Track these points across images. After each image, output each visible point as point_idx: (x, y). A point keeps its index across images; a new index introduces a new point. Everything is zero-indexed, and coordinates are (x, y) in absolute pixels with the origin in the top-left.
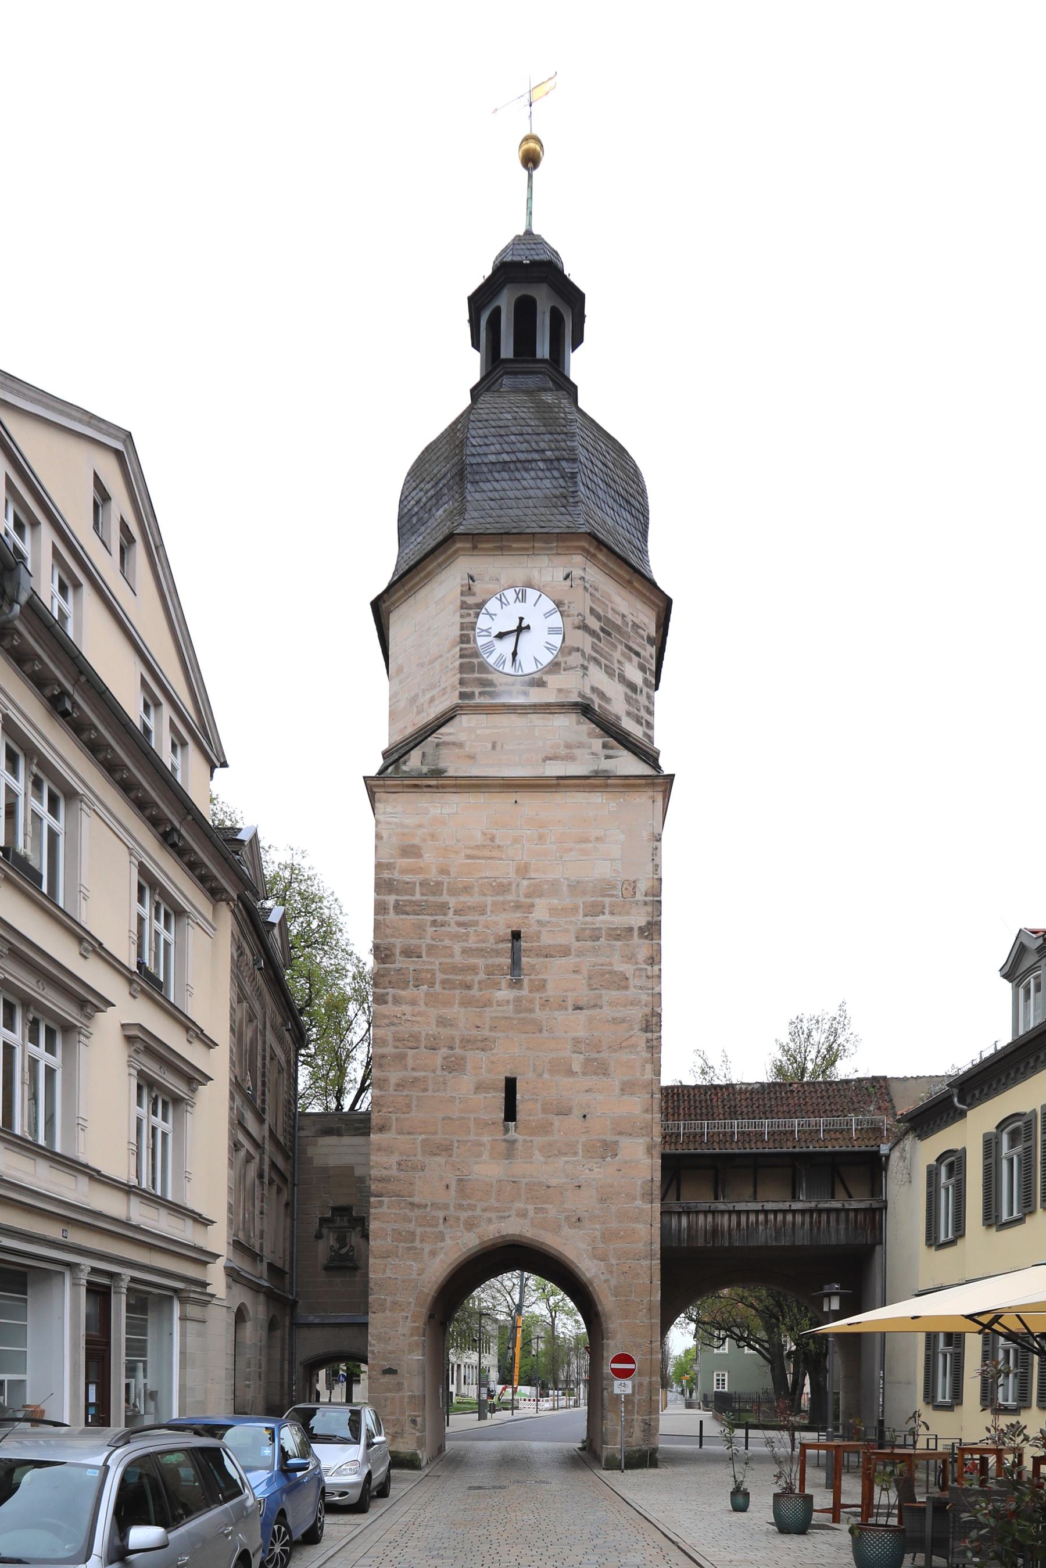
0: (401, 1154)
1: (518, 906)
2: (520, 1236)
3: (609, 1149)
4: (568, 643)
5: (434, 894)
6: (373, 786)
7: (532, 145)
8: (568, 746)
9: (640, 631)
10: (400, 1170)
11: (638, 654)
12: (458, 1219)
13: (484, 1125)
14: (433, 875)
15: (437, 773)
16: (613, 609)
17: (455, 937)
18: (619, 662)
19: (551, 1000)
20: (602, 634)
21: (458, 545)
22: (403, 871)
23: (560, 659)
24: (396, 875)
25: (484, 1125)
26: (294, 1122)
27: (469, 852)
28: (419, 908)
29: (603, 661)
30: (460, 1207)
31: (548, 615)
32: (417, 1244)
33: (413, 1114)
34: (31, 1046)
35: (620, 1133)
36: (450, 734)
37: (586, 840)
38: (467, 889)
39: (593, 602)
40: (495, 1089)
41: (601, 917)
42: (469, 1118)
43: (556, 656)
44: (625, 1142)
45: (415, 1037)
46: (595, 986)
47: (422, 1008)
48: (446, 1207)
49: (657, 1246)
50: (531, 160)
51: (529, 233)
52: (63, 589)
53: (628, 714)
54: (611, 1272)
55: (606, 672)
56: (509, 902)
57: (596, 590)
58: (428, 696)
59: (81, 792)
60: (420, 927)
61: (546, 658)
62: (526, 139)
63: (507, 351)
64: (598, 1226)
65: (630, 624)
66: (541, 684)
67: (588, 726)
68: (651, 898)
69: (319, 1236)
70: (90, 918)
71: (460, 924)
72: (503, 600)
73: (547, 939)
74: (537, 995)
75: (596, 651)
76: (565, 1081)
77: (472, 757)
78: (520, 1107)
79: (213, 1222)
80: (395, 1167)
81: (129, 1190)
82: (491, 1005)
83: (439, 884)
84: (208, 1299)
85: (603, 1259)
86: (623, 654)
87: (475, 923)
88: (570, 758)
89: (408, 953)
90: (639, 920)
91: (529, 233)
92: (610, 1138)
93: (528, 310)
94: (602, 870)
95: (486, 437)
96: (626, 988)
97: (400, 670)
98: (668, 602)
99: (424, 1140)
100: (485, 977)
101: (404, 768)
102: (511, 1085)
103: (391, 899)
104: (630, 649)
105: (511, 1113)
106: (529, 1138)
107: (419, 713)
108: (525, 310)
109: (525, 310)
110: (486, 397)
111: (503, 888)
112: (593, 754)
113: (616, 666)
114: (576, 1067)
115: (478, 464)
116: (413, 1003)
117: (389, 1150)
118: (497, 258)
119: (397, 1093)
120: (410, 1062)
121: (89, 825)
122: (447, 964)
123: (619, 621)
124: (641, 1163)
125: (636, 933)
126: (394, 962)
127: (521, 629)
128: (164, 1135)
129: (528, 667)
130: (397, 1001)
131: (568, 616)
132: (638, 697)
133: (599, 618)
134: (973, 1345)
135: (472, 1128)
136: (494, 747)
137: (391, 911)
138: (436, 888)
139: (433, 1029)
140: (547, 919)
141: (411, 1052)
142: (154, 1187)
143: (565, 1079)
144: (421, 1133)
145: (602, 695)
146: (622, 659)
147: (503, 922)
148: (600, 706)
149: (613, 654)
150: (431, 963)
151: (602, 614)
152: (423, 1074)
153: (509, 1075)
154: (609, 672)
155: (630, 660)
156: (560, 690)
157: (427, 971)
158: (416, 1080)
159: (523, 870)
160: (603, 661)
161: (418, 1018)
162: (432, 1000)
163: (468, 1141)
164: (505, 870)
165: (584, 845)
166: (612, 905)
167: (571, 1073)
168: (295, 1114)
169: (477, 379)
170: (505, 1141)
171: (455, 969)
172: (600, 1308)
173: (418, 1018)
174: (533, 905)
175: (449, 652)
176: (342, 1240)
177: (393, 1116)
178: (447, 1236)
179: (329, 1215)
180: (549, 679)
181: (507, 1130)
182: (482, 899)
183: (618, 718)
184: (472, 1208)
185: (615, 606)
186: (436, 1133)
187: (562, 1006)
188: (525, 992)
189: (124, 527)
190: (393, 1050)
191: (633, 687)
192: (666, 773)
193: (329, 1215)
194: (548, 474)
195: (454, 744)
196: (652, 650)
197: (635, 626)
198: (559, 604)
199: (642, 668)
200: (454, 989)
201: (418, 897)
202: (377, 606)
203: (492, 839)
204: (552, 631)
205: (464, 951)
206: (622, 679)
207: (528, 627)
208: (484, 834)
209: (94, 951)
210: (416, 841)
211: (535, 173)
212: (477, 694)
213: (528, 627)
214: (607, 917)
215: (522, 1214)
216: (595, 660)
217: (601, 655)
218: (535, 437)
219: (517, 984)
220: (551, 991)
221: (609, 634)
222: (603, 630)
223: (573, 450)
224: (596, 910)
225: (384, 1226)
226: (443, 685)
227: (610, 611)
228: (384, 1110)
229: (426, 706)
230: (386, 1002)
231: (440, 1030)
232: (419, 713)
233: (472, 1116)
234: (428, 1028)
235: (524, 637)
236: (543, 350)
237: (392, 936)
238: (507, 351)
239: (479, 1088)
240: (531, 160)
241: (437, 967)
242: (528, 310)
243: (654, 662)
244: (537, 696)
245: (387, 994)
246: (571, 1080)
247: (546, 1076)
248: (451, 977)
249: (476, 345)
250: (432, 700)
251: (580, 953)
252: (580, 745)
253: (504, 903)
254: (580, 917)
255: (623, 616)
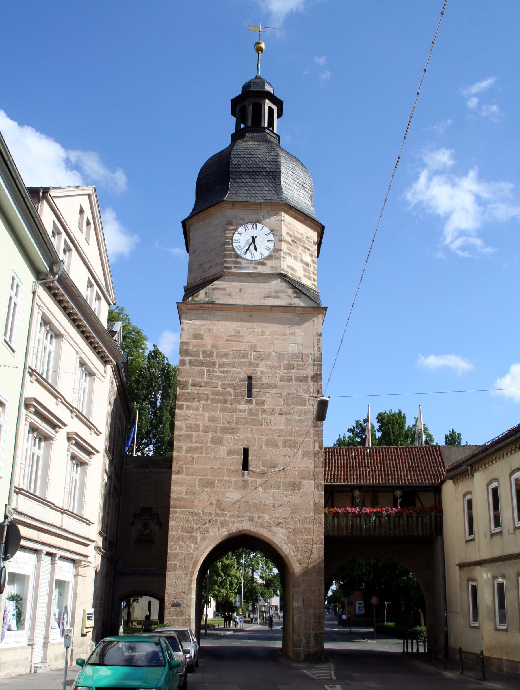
0: (188, 486)
1: (251, 364)
2: (249, 531)
3: (295, 486)
4: (276, 247)
5: (209, 357)
8: (276, 292)
9: (310, 240)
10: (186, 494)
11: (309, 250)
12: (217, 521)
13: (231, 472)
14: (209, 348)
15: (212, 303)
16: (297, 232)
17: (219, 378)
18: (300, 254)
19: (267, 410)
20: (292, 243)
21: (225, 205)
22: (194, 346)
23: (272, 253)
24: (191, 347)
25: (231, 472)
26: (123, 460)
27: (227, 338)
28: (201, 364)
29: (293, 254)
30: (218, 515)
32: (194, 534)
33: (195, 466)
34: (33, 447)
35: (302, 478)
36: (220, 284)
37: (284, 335)
38: (226, 355)
39: (288, 229)
40: (238, 454)
41: (292, 371)
42: (223, 469)
43: (271, 253)
44: (305, 482)
45: (198, 426)
46: (289, 404)
47: (201, 411)
48: (210, 514)
49: (323, 537)
52: (65, 251)
53: (305, 276)
54: (298, 551)
55: (294, 259)
56: (247, 362)
57: (289, 224)
58: (208, 265)
59: (63, 334)
60: (202, 373)
61: (266, 253)
64: (291, 527)
65: (305, 237)
66: (263, 264)
67: (284, 284)
68: (317, 363)
69: (133, 524)
70: (62, 388)
71: (221, 372)
72: (246, 228)
73: (265, 380)
74: (260, 407)
75: (289, 250)
76: (274, 450)
77: (230, 295)
78: (250, 463)
79: (93, 524)
80: (184, 492)
81: (63, 512)
82: (236, 412)
83: (211, 352)
84: (88, 564)
85: (294, 543)
86: (302, 250)
87: (230, 372)
88: (276, 297)
89: (194, 385)
90: (310, 371)
92: (297, 480)
94: (293, 348)
95: (240, 161)
96: (305, 405)
97: (195, 251)
99: (200, 479)
100: (233, 397)
101: (196, 299)
102: (246, 452)
103: (188, 359)
104: (305, 248)
105: (246, 466)
106: (254, 479)
107: (203, 272)
111: (244, 356)
112: (288, 296)
113: (299, 256)
114: (280, 444)
115: (235, 172)
116: (197, 409)
117: (181, 484)
119: (187, 455)
120: (194, 439)
121: (65, 345)
122: (214, 390)
123: (300, 237)
124: (312, 494)
125: (309, 379)
126: (188, 389)
128: (38, 457)
129: (257, 256)
130: (188, 408)
131: (277, 236)
132: (309, 268)
133: (291, 236)
134: (323, 659)
135: (225, 473)
136: (240, 291)
137: (187, 364)
138: (211, 355)
139: (206, 422)
140: (266, 371)
141: (194, 434)
142: (30, 489)
143: (273, 450)
144: (198, 476)
145: (292, 269)
146: (301, 253)
147: (242, 373)
148: (291, 274)
149: (297, 250)
150: (206, 390)
151: (292, 234)
152: (200, 445)
153: (245, 447)
154: (296, 258)
155: (305, 252)
156: (272, 267)
157: (204, 394)
158: (196, 448)
159: (253, 348)
160: (293, 254)
161: (199, 417)
162: (206, 408)
163: (222, 480)
164: (245, 347)
165: (284, 337)
166: (298, 365)
167: (277, 446)
168: (123, 457)
170: (243, 480)
171: (218, 393)
172: (291, 571)
173: (199, 417)
174: (258, 364)
175: (220, 248)
176: (146, 525)
177: (184, 466)
178: (210, 530)
179: (139, 512)
180: (268, 262)
181: (243, 475)
182: (233, 360)
183: (300, 278)
184: (225, 515)
185: (298, 231)
186: (206, 476)
187: (272, 412)
188: (254, 405)
189: (88, 220)
190: (186, 433)
191: (307, 264)
192: (323, 306)
193: (139, 512)
194: (267, 177)
195: (221, 289)
196: (316, 247)
197: (308, 238)
198: (272, 231)
199: (311, 255)
200: (218, 403)
201: (201, 358)
202: (184, 223)
203: (239, 332)
205: (223, 385)
206: (302, 261)
208: (235, 330)
209: (62, 403)
210: (202, 332)
212: (233, 267)
214: (294, 371)
215: (251, 519)
216: (289, 254)
217: (292, 252)
218: (262, 163)
219: (251, 402)
220: (266, 406)
221: (295, 242)
222: (292, 241)
224: (290, 367)
225: (177, 524)
226: (216, 262)
227: (296, 232)
228: (179, 463)
229: (207, 269)
230: (183, 409)
231: (209, 423)
232: (203, 272)
233: (225, 467)
234: (204, 422)
237: (187, 377)
239: (229, 453)
241: (209, 393)
243: (316, 252)
244: (261, 269)
245: (184, 405)
246: (277, 450)
247: (264, 447)
248: (217, 397)
250: (210, 267)
251: (282, 388)
252: (282, 292)
253: (244, 362)
254: (282, 370)
255: (302, 234)
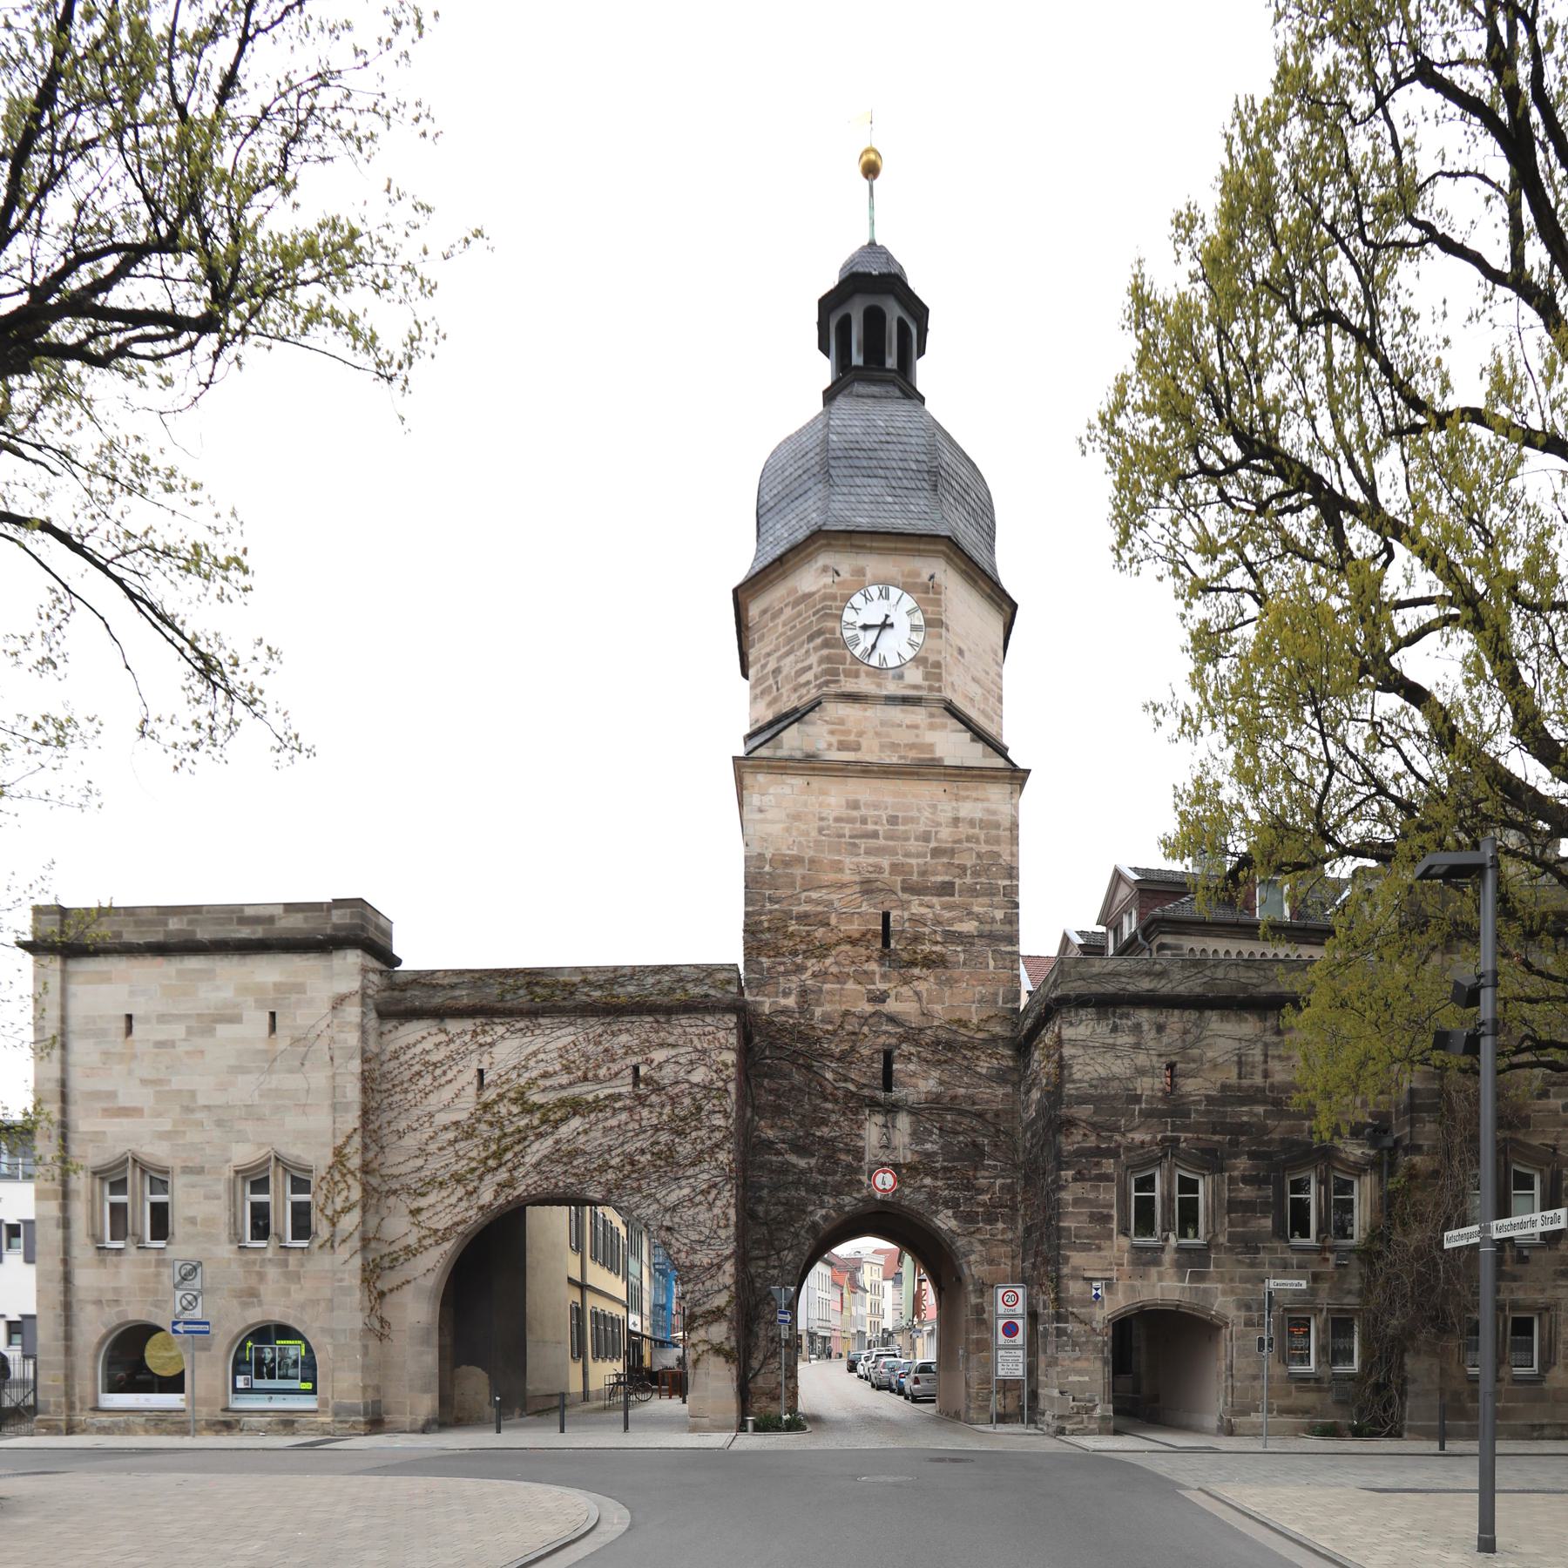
6: (743, 766)
7: (872, 156)
31: (909, 613)
50: (871, 170)
51: (872, 244)
61: (893, 662)
62: (867, 151)
63: (857, 359)
91: (872, 244)
93: (872, 324)
98: (1014, 606)
108: (874, 319)
109: (874, 319)
110: (840, 402)
118: (844, 267)
127: (885, 625)
169: (828, 383)
204: (914, 628)
207: (892, 625)
211: (875, 182)
213: (892, 625)
223: (1440, 1323)
235: (887, 633)
236: (891, 362)
238: (857, 359)
240: (871, 170)
242: (872, 324)
249: (824, 347)
